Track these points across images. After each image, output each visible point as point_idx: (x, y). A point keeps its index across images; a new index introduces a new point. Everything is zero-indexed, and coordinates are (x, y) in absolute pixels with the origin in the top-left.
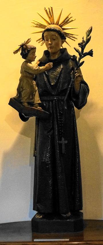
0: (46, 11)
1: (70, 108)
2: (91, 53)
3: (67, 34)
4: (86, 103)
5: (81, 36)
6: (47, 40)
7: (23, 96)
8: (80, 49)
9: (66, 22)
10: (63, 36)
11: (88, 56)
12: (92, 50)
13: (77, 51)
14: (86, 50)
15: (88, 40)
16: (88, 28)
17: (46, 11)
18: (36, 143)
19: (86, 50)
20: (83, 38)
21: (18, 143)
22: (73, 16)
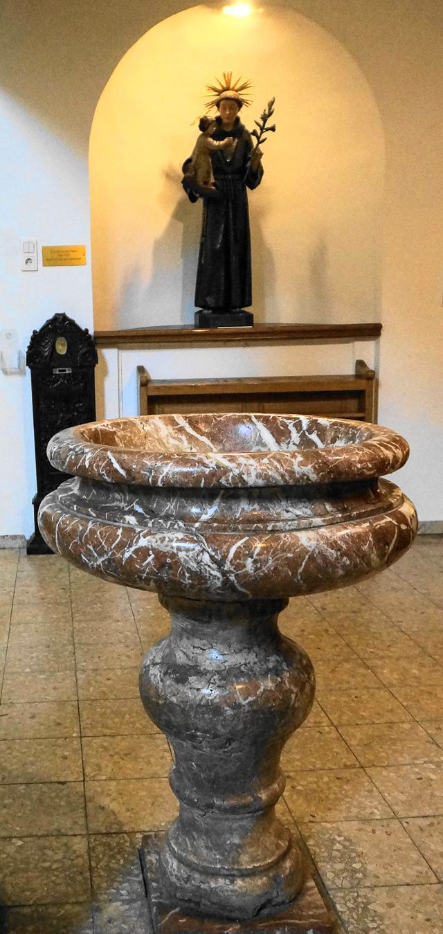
0: (224, 75)
1: (244, 189)
2: (273, 129)
3: (243, 100)
4: (259, 183)
5: (263, 108)
6: (225, 109)
7: (199, 173)
8: (261, 123)
9: (242, 88)
10: (239, 103)
11: (270, 132)
12: (231, 103)
13: (258, 125)
14: (267, 126)
15: (270, 114)
16: (270, 99)
17: (224, 75)
18: (295, 332)
19: (267, 126)
20: (265, 111)
21: (171, 226)
22: (227, 71)
